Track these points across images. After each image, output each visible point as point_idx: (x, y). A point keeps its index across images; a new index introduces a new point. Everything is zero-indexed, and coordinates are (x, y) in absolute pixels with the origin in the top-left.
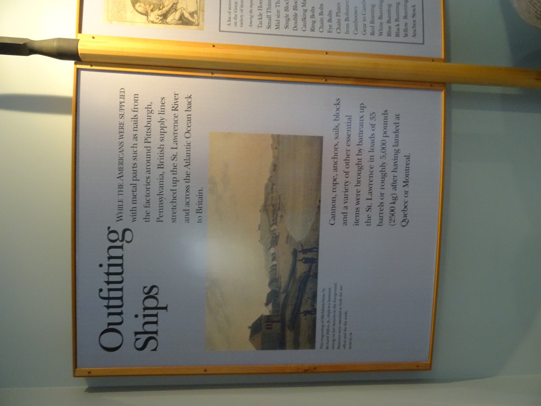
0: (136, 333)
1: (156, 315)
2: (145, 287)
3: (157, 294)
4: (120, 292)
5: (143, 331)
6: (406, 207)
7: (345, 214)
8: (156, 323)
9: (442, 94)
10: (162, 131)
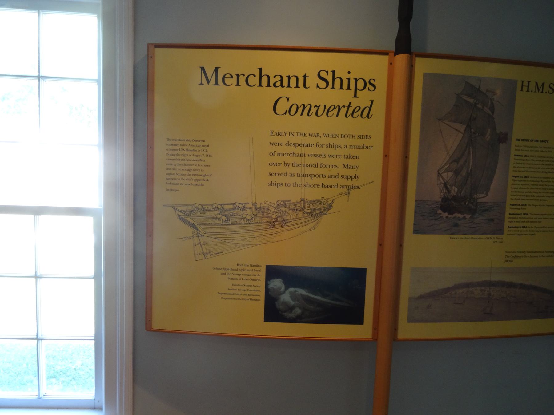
0: (333, 72)
1: (349, 88)
2: (375, 80)
3: (369, 90)
4: (287, 85)
6: (367, 148)
9: (498, 132)
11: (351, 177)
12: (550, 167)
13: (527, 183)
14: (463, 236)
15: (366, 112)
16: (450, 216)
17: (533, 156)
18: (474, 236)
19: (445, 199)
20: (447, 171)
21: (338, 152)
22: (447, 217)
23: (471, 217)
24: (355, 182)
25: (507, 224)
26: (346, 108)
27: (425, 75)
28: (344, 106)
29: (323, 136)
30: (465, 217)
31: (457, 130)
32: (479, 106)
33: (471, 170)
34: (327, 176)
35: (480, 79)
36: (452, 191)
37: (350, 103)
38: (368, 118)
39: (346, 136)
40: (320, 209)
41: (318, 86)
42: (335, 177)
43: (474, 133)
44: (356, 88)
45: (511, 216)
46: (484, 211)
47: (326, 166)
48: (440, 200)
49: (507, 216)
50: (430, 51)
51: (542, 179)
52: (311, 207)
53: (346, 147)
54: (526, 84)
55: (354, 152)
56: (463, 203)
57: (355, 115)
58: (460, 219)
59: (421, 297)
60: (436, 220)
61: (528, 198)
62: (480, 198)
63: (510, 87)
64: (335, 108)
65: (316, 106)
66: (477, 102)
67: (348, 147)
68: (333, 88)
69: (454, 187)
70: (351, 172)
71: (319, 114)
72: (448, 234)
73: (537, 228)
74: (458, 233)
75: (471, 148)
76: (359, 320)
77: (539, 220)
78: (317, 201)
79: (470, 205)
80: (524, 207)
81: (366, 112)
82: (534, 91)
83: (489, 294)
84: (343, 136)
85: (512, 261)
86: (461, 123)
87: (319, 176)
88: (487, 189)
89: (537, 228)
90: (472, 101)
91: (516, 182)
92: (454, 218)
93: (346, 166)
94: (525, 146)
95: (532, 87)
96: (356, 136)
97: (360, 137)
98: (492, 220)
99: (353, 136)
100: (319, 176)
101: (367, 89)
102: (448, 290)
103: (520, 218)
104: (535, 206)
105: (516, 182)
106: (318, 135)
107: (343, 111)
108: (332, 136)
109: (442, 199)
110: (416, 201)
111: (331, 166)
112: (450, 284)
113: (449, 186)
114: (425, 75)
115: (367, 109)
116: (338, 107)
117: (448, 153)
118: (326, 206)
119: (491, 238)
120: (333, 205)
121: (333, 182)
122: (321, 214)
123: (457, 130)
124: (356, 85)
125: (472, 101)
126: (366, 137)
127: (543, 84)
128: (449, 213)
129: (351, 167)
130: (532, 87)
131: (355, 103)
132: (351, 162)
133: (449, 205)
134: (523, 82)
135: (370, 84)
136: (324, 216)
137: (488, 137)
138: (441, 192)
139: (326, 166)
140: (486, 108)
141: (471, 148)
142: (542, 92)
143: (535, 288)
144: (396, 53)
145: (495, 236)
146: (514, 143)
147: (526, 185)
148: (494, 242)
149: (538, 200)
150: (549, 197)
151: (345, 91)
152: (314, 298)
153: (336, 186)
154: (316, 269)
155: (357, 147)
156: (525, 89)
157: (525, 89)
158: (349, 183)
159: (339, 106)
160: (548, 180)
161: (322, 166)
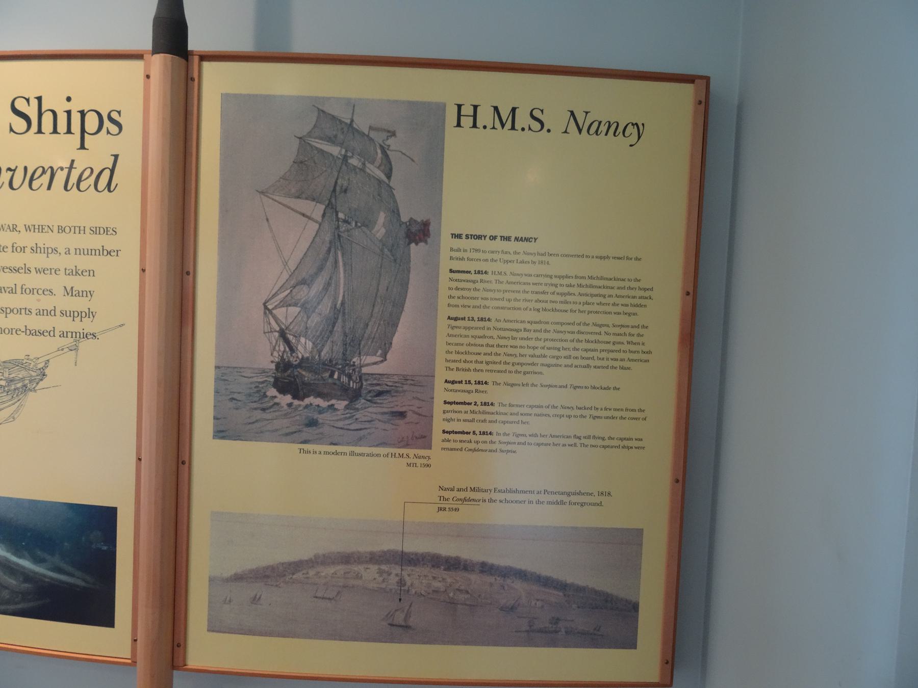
0: (39, 99)
1: (69, 131)
2: (119, 112)
3: (108, 132)
5: (43, 110)
6: (109, 253)
7: (53, 313)
8: (55, 131)
9: (405, 218)
10: (76, 314)
11: (80, 314)
12: (569, 298)
13: (488, 333)
14: (333, 448)
15: (106, 179)
16: (296, 402)
17: (500, 273)
18: (358, 450)
19: (283, 366)
20: (284, 303)
21: (53, 261)
22: (290, 405)
23: (347, 407)
24: (87, 326)
25: (438, 425)
26: (66, 171)
27: (226, 98)
28: (62, 169)
29: (23, 230)
30: (333, 405)
31: (303, 215)
32: (354, 161)
33: (343, 304)
34: (34, 312)
35: (352, 105)
36: (300, 347)
37: (73, 161)
38: (109, 191)
39: (67, 230)
40: (22, 379)
41: (11, 130)
42: (49, 313)
43: (345, 221)
44: (83, 131)
45: (448, 407)
46: (380, 394)
47: (32, 291)
48: (273, 366)
49: (438, 407)
50: (299, 47)
51: (528, 326)
52: (6, 375)
53: (68, 252)
54: (467, 110)
55: (84, 262)
56: (327, 375)
57: (83, 186)
58: (321, 410)
59: (238, 578)
60: (264, 410)
61: (490, 367)
62: (367, 365)
63: (428, 120)
64: (44, 172)
65: (9, 169)
66: (349, 154)
67: (72, 251)
68: (40, 131)
69: (303, 340)
70: (79, 304)
71: (16, 184)
72: (293, 442)
73: (518, 436)
74: (318, 440)
75: (340, 253)
76: (106, 619)
77: (525, 419)
78: (17, 364)
79: (344, 379)
80: (480, 387)
81: (106, 179)
82: (490, 126)
83: (401, 583)
84: (61, 229)
85: (457, 510)
86: (314, 200)
87: (19, 311)
88: (385, 347)
89: (518, 436)
90: (335, 150)
91: (456, 332)
92: (306, 407)
93: (70, 292)
94: (477, 250)
95: (486, 116)
96: (87, 230)
97: (95, 231)
98: (402, 415)
99: (81, 230)
100: (19, 311)
101: (104, 130)
102: (297, 566)
103: (473, 412)
104: (512, 385)
105: (456, 332)
106: (14, 228)
107: (60, 177)
108: (41, 229)
109: (278, 365)
110: (217, 367)
111: (40, 292)
112: (304, 553)
113: (291, 337)
114: (226, 98)
115: (107, 173)
116: (49, 171)
117: (285, 264)
118: (34, 374)
119: (401, 456)
120: (47, 371)
121: (44, 323)
122: (25, 389)
123: (303, 215)
124: (84, 124)
125: (335, 150)
126: (106, 231)
127: (514, 110)
128: (295, 397)
129: (80, 294)
130: (486, 116)
131: (83, 161)
132: (79, 283)
133: (290, 379)
134: (459, 106)
135: (110, 121)
136: (31, 394)
137: (379, 230)
138: (274, 349)
139: (32, 291)
140: (371, 167)
141: (340, 253)
142: (513, 128)
143: (522, 575)
144: (153, 54)
145: (412, 452)
146: (446, 242)
147: (484, 337)
148: (409, 465)
149: (517, 372)
150: (548, 366)
151: (62, 138)
152: (18, 565)
153: (51, 333)
154: (19, 502)
155: (91, 252)
156: (467, 122)
157: (467, 122)
158: (76, 326)
159: (51, 168)
160: (543, 327)
161: (24, 291)
